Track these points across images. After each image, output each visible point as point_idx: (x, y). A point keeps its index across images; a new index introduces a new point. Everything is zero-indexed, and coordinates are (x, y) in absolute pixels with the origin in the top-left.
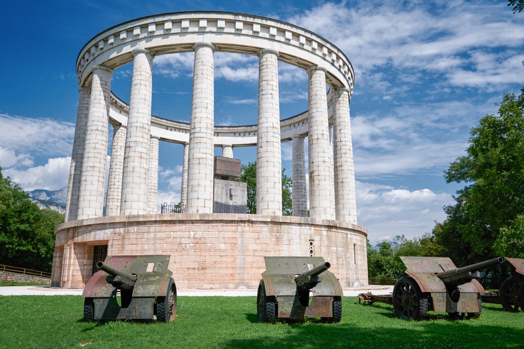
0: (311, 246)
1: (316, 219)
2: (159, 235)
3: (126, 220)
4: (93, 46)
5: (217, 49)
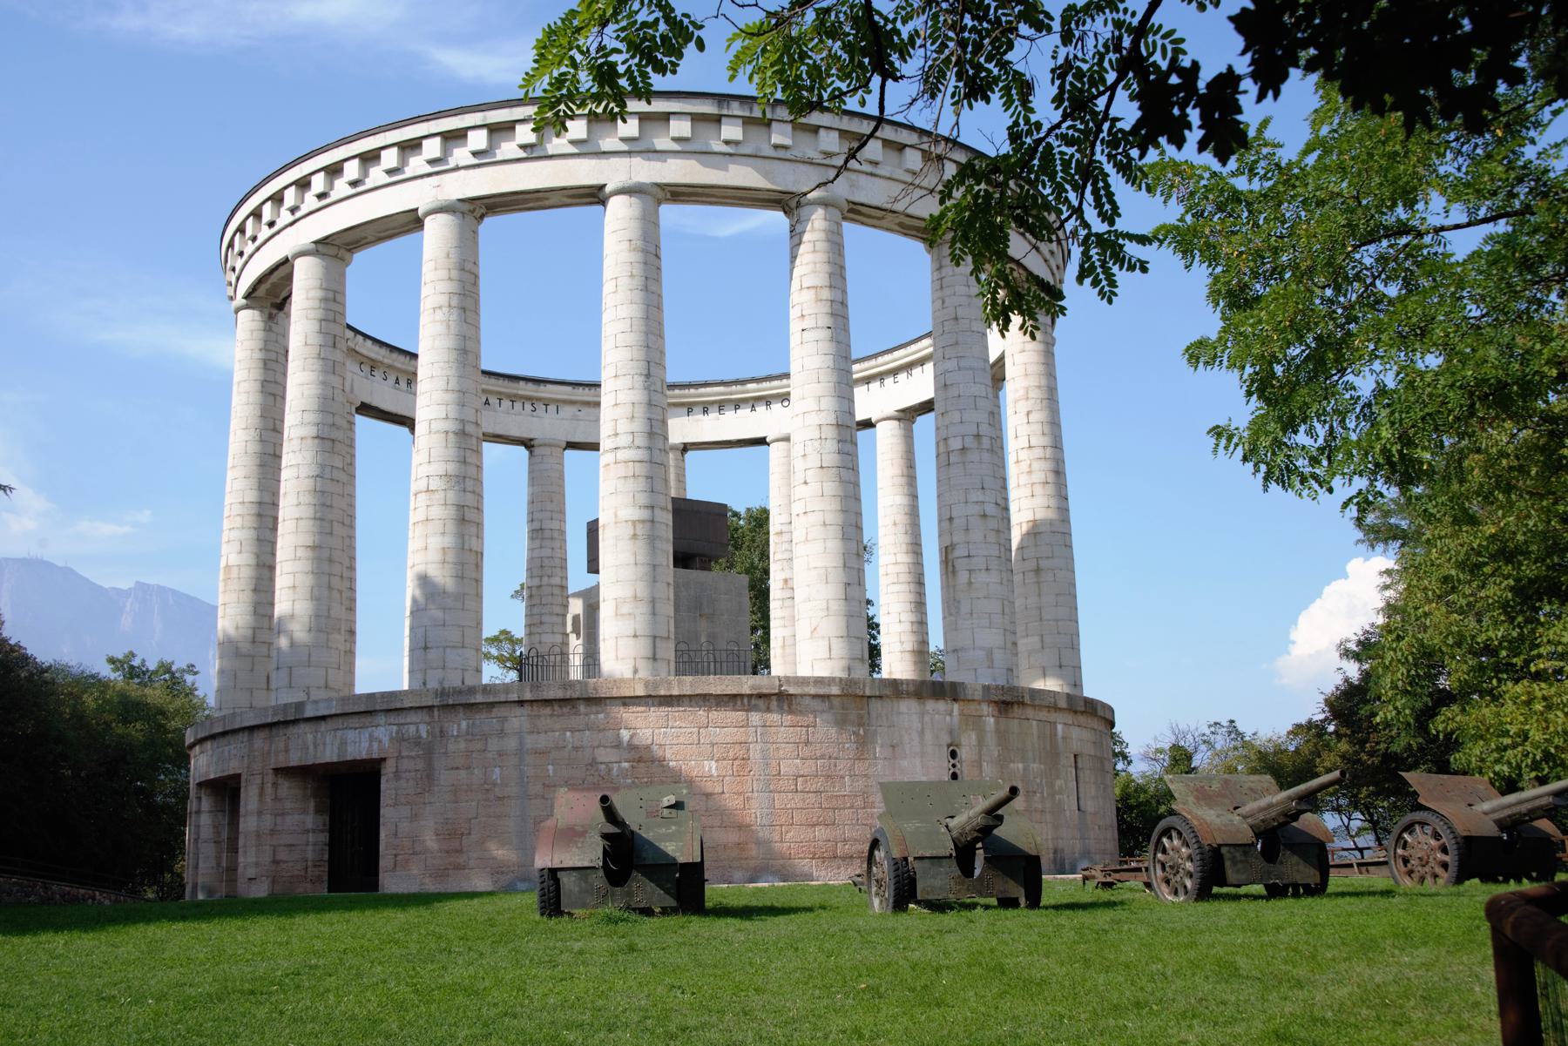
0: (952, 761)
1: (833, 731)
2: (530, 741)
3: (436, 702)
4: (290, 185)
5: (669, 196)
